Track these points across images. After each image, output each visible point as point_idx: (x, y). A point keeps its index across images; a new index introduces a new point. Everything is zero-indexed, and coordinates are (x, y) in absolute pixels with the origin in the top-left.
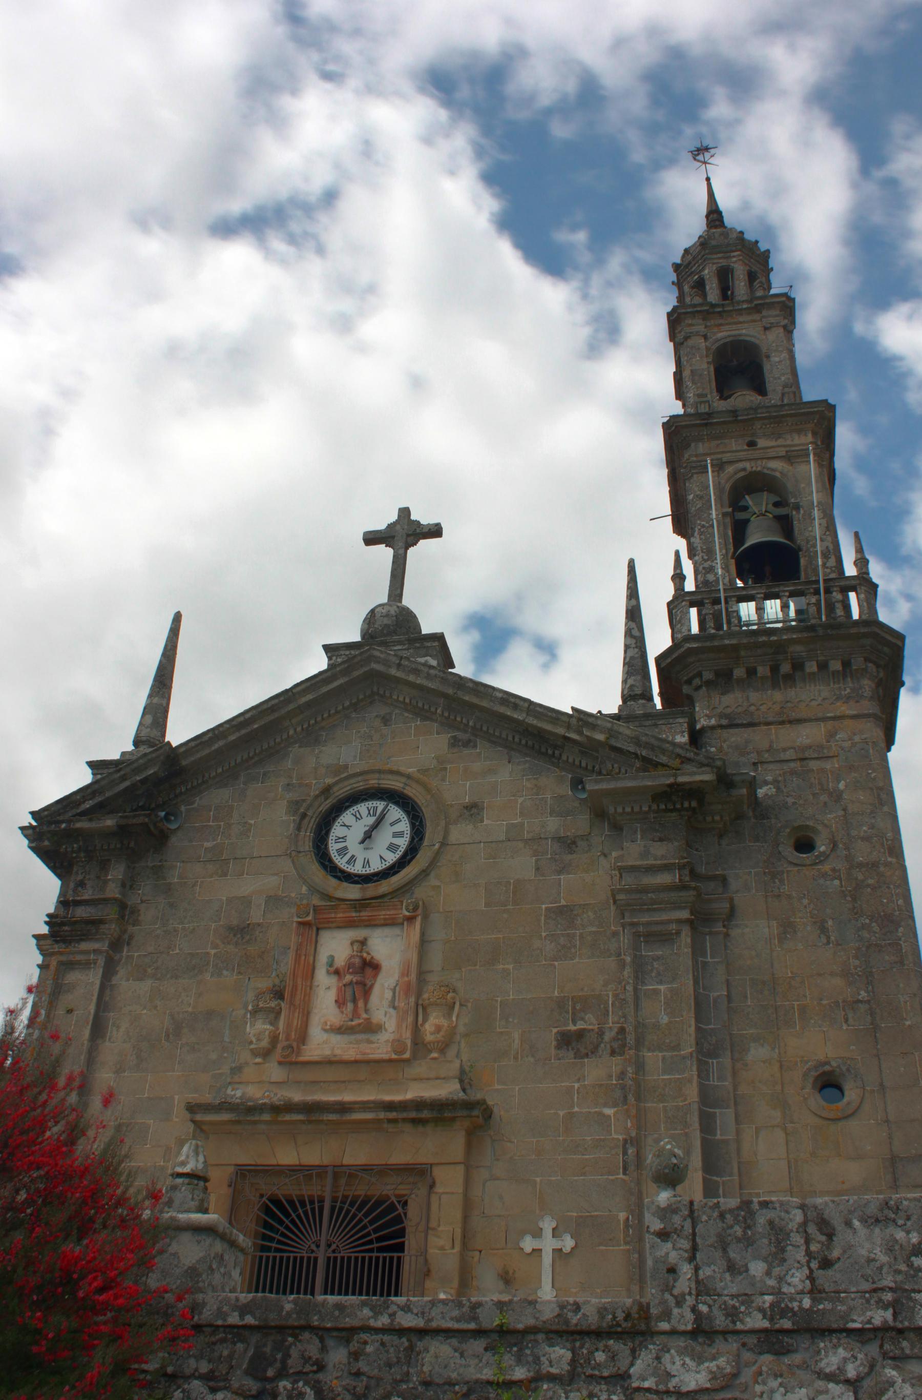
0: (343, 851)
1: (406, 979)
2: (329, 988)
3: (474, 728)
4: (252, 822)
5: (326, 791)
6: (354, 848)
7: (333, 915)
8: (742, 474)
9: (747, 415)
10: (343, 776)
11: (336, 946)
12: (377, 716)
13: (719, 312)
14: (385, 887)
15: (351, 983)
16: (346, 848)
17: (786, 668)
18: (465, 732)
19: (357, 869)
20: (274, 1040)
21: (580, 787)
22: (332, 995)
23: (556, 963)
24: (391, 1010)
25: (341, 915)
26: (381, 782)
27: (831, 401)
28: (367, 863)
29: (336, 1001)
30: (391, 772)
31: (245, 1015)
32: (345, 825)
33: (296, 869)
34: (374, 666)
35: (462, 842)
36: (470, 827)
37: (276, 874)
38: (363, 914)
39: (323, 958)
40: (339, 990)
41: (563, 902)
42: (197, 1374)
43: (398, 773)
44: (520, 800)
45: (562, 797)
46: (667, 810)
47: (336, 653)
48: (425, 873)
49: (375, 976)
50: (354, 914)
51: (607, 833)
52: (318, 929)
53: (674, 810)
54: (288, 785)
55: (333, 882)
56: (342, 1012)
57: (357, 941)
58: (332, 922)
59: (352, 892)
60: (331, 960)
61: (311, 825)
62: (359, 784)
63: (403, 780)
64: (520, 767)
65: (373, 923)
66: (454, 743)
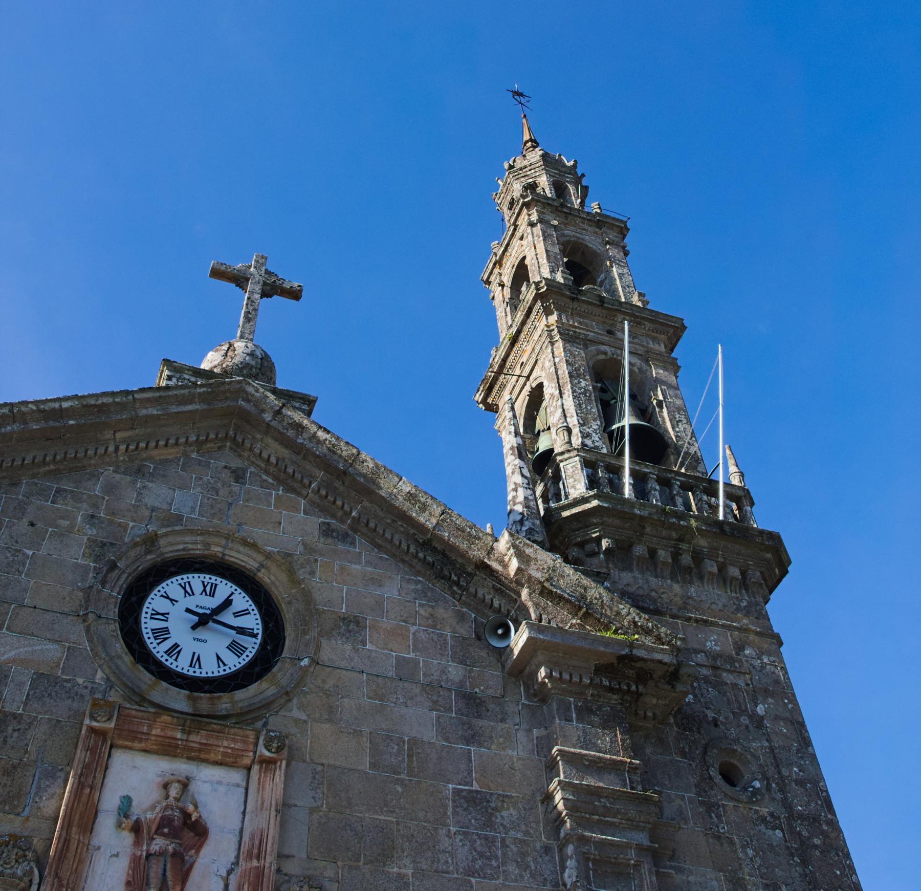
0: (162, 634)
1: (255, 863)
2: (117, 855)
3: (357, 520)
4: (30, 553)
5: (151, 541)
6: (180, 630)
8: (602, 357)
9: (612, 305)
10: (177, 528)
11: (136, 778)
12: (225, 467)
13: (565, 213)
14: (225, 703)
15: (162, 853)
16: (166, 630)
17: (686, 559)
18: (342, 521)
19: (182, 665)
21: (500, 632)
23: (473, 880)
26: (227, 552)
27: (686, 323)
28: (196, 660)
30: (245, 542)
32: (168, 598)
33: (90, 641)
34: (241, 402)
35: (336, 664)
36: (348, 647)
37: (56, 641)
38: (193, 738)
39: (110, 801)
40: (135, 861)
41: (476, 787)
43: (254, 546)
44: (413, 629)
45: (464, 639)
46: (610, 689)
47: (178, 375)
48: (287, 695)
49: (199, 847)
51: (524, 701)
53: (620, 690)
54: (93, 516)
55: (147, 677)
57: (179, 781)
58: (141, 740)
59: (178, 699)
60: (127, 801)
61: (120, 582)
62: (194, 546)
63: (260, 558)
64: (412, 587)
65: (203, 756)
66: (326, 531)
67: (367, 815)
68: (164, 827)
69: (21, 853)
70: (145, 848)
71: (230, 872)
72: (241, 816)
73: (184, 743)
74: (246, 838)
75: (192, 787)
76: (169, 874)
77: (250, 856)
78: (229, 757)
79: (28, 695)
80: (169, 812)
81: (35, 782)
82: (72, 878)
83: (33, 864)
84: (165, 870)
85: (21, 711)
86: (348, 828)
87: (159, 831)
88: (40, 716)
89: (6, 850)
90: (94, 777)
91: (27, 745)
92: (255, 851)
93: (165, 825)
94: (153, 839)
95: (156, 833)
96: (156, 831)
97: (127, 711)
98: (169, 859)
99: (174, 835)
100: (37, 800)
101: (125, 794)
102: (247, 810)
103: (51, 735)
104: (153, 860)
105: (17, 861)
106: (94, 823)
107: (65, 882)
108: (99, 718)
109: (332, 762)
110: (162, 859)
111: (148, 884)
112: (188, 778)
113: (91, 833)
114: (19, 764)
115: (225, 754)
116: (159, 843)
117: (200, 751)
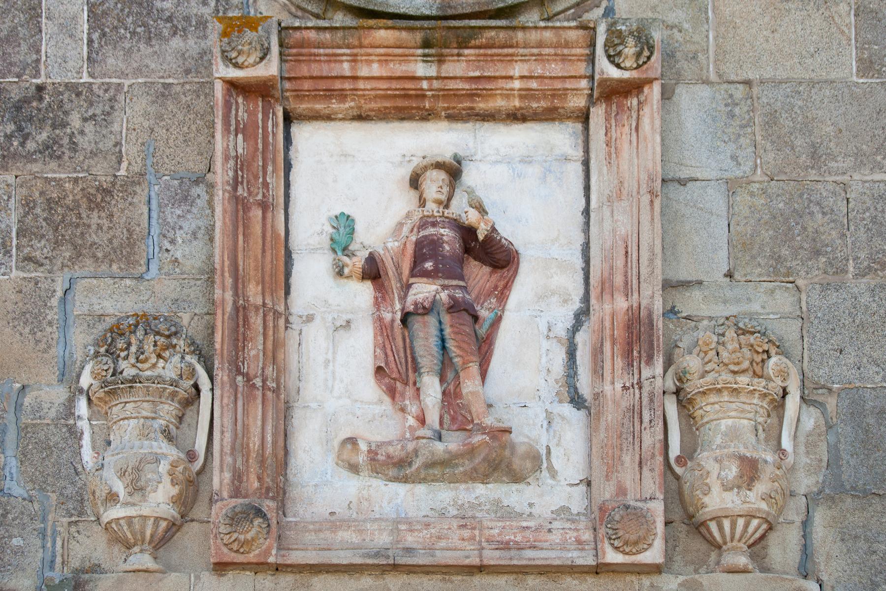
7: (346, 69)
20: (191, 489)
22: (361, 347)
24: (567, 409)
25: (376, 70)
29: (379, 370)
31: (70, 403)
39: (309, 227)
40: (383, 328)
42: (234, 61)
50: (421, 69)
52: (288, 119)
56: (403, 410)
57: (439, 166)
58: (342, 96)
60: (344, 226)
65: (481, 105)
67: (856, 176)
68: (425, 260)
69: (161, 340)
70: (398, 306)
71: (575, 329)
72: (581, 219)
73: (436, 84)
74: (595, 262)
75: (471, 177)
76: (450, 344)
77: (607, 287)
78: (538, 100)
79: (90, 42)
80: (431, 231)
81: (154, 215)
82: (269, 371)
83: (191, 359)
84: (443, 340)
85: (85, 79)
86: (816, 209)
87: (417, 271)
88: (127, 83)
89: (133, 340)
90: (266, 185)
91: (117, 144)
92: (619, 280)
93: (425, 255)
94: (409, 286)
95: (412, 275)
96: (412, 270)
97: (298, 35)
98: (446, 318)
99: (448, 270)
100: (167, 245)
101: (337, 212)
102: (593, 204)
103: (160, 117)
104: (417, 324)
105: (159, 356)
106: (288, 275)
107: (258, 382)
108: (240, 60)
109: (768, 73)
110: (432, 320)
111: (416, 369)
112: (458, 160)
113: (287, 292)
114: (113, 184)
115: (527, 94)
116: (424, 290)
117: (472, 95)
